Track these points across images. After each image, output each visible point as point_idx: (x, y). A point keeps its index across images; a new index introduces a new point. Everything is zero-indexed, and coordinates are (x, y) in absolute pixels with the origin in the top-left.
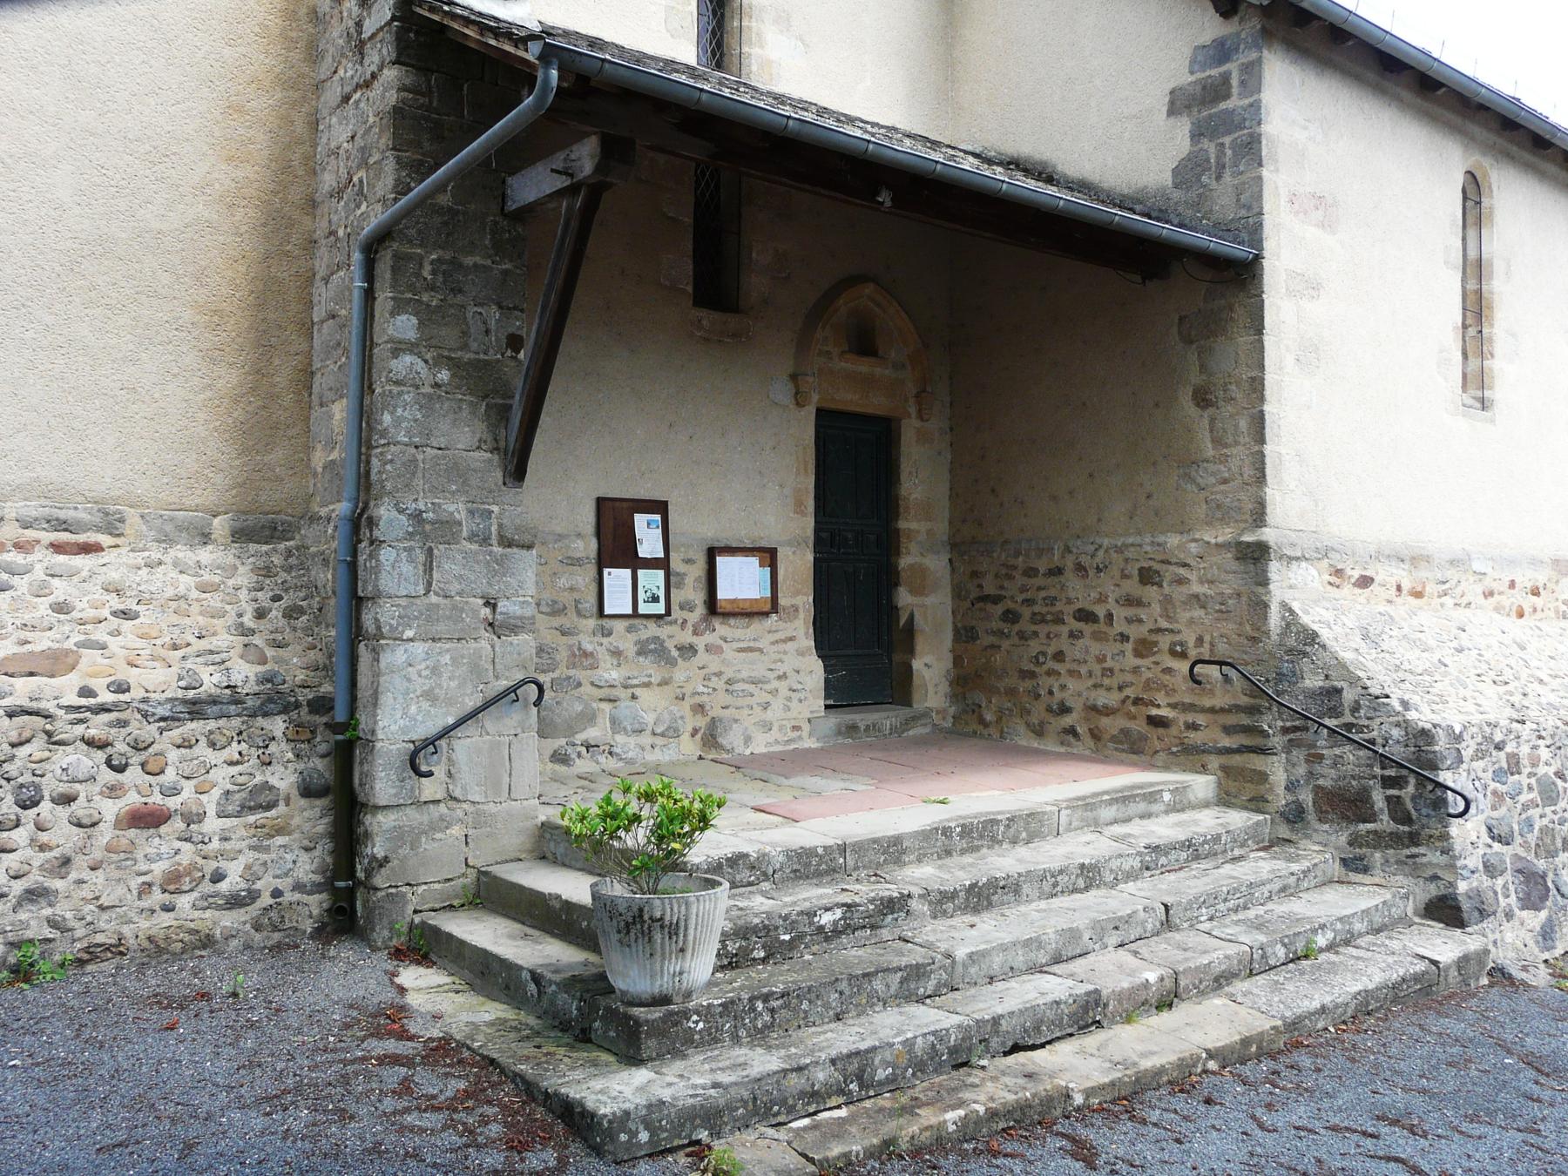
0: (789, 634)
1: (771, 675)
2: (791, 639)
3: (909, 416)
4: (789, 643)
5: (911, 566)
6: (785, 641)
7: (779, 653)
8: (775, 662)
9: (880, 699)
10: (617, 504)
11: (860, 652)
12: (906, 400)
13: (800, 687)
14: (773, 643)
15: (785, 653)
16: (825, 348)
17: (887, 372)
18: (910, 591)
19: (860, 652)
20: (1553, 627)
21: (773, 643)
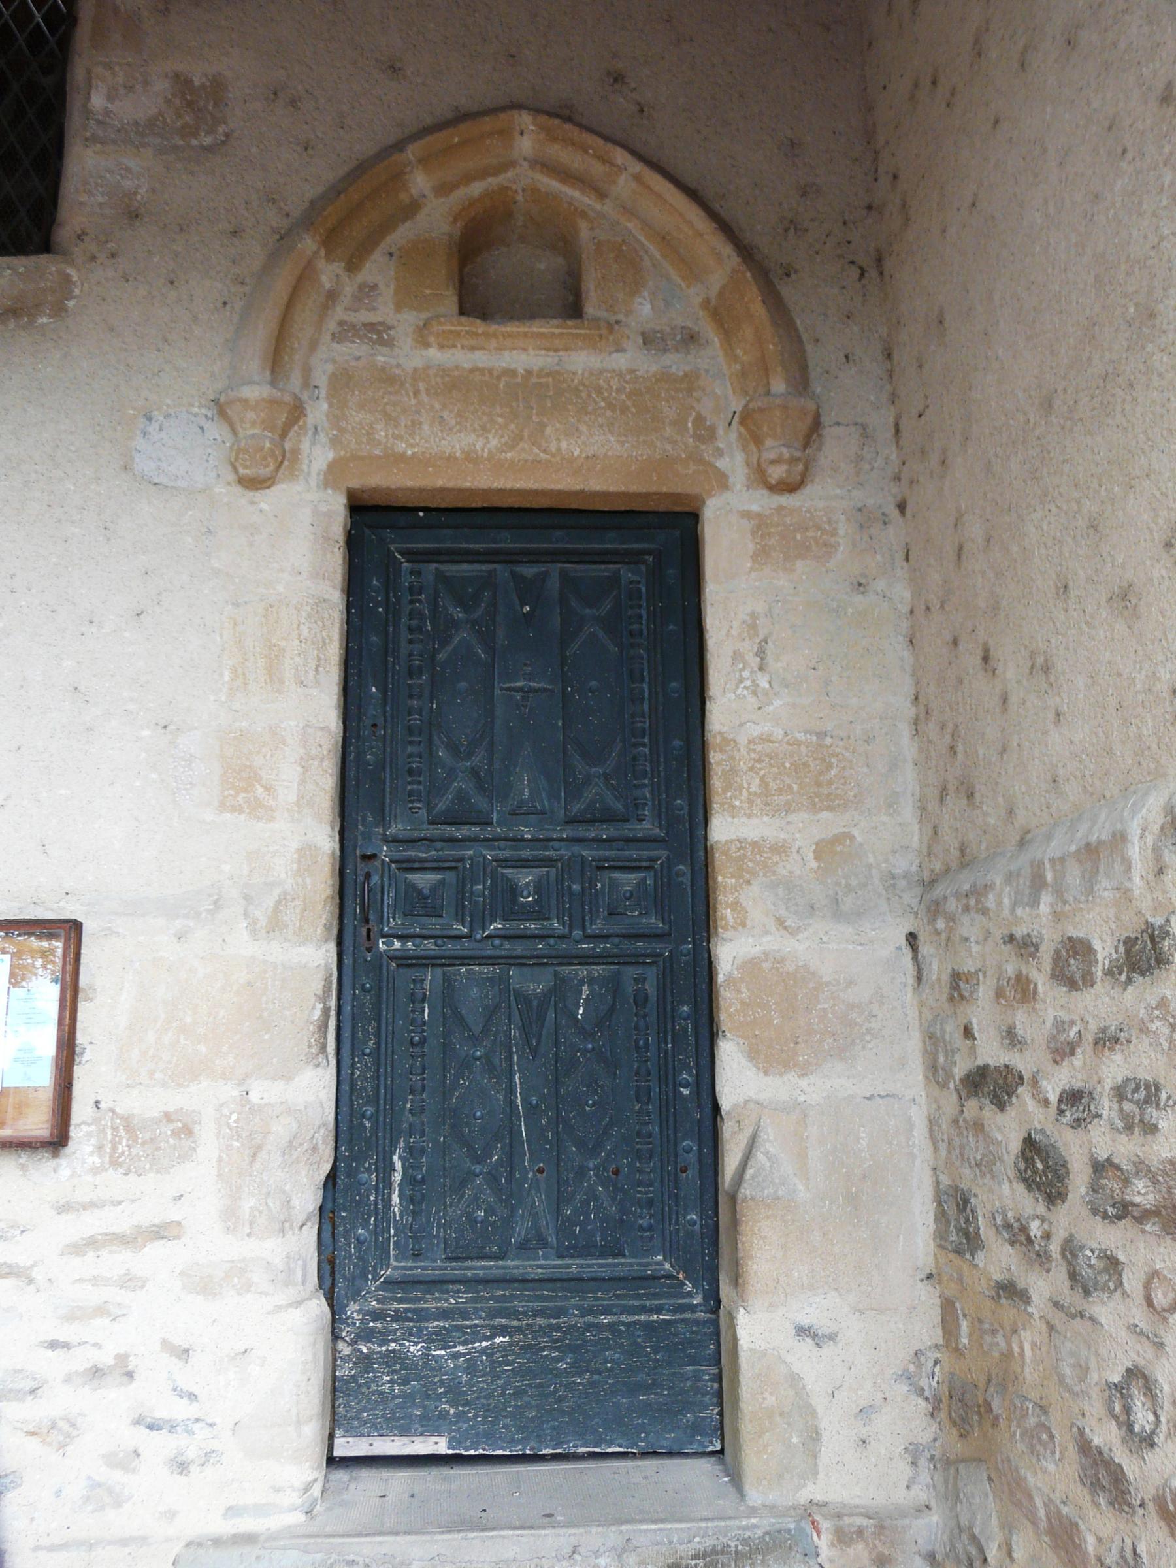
0: (148, 1214)
1: (52, 1365)
2: (160, 1232)
3: (723, 482)
4: (156, 1250)
5: (751, 966)
6: (132, 1240)
7: (96, 1281)
8: (74, 1315)
9: (667, 1440)
10: (700, 731)
11: (574, 1266)
12: (706, 434)
13: (181, 1410)
14: (78, 1249)
15: (130, 1282)
16: (364, 316)
17: (621, 361)
18: (753, 1055)
19: (574, 1266)
20: (1170, 1447)
21: (78, 1249)
